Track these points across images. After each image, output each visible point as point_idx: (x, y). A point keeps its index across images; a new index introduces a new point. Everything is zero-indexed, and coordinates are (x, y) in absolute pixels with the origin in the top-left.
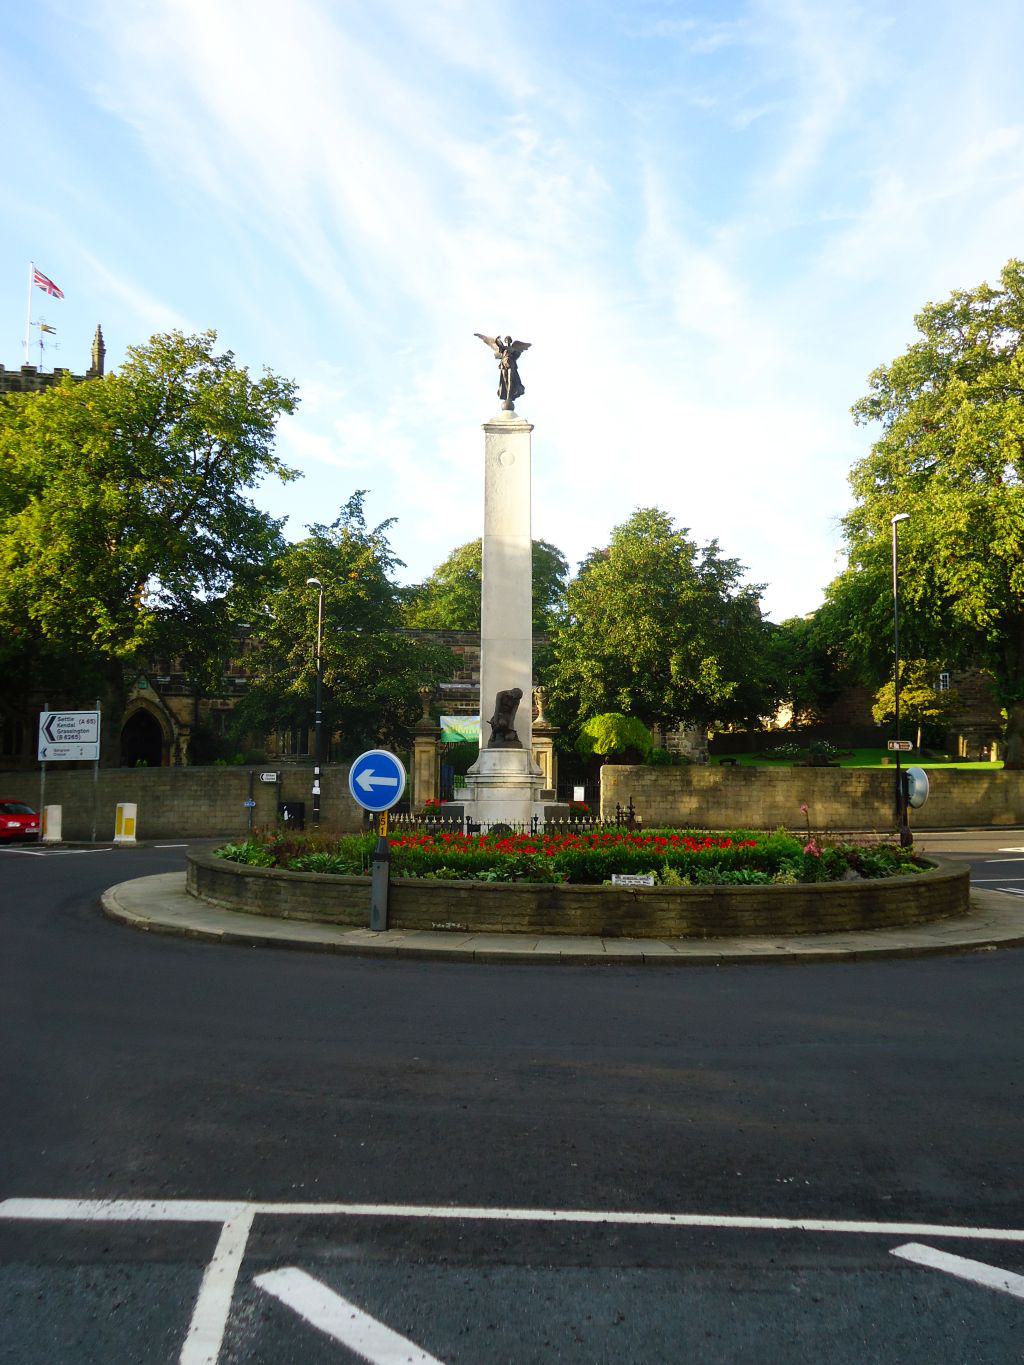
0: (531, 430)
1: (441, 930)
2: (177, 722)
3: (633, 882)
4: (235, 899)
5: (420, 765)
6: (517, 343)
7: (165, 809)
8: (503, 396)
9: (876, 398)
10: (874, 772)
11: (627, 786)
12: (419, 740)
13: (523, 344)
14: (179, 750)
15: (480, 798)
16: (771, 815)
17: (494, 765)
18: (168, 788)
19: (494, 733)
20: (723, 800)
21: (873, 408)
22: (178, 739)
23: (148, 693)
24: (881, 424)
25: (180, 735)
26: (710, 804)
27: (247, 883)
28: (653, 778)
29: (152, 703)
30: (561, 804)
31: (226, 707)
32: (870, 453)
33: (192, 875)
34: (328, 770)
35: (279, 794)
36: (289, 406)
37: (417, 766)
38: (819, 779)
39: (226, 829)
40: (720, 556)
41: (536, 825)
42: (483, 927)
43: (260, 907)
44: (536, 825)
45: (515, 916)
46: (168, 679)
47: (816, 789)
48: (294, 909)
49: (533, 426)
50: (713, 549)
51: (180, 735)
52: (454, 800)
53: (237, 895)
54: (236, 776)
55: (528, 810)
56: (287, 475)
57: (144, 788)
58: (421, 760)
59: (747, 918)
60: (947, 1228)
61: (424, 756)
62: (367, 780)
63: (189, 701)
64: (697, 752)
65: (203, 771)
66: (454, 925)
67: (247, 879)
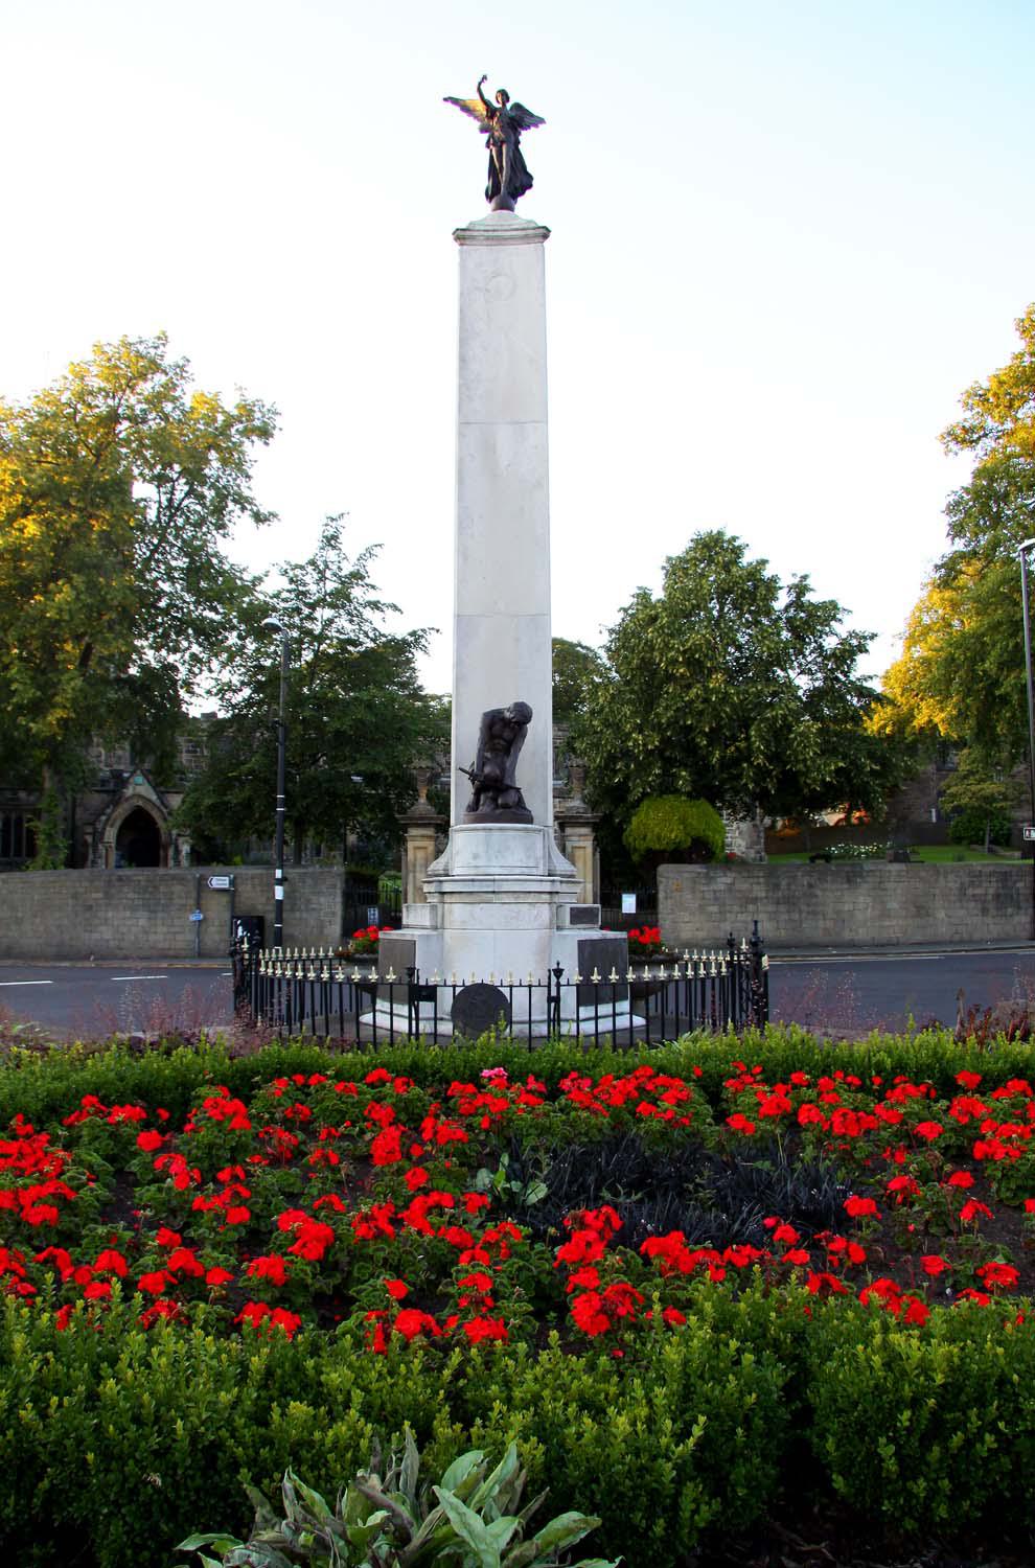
5: (414, 866)
9: (967, 425)
10: (1008, 869)
11: (694, 892)
12: (413, 832)
13: (532, 115)
14: (177, 851)
15: (447, 925)
16: (882, 927)
18: (100, 895)
19: (477, 794)
20: (820, 908)
21: (966, 437)
24: (973, 454)
25: (179, 835)
26: (804, 915)
28: (729, 881)
29: (150, 801)
30: (610, 934)
32: (970, 481)
34: (293, 873)
35: (233, 905)
36: (265, 433)
37: (411, 868)
38: (941, 879)
39: (169, 949)
40: (809, 597)
41: (558, 985)
44: (558, 985)
47: (937, 891)
50: (801, 589)
51: (179, 835)
54: (181, 880)
55: (546, 949)
56: (259, 518)
57: (75, 896)
58: (415, 860)
64: (752, 851)
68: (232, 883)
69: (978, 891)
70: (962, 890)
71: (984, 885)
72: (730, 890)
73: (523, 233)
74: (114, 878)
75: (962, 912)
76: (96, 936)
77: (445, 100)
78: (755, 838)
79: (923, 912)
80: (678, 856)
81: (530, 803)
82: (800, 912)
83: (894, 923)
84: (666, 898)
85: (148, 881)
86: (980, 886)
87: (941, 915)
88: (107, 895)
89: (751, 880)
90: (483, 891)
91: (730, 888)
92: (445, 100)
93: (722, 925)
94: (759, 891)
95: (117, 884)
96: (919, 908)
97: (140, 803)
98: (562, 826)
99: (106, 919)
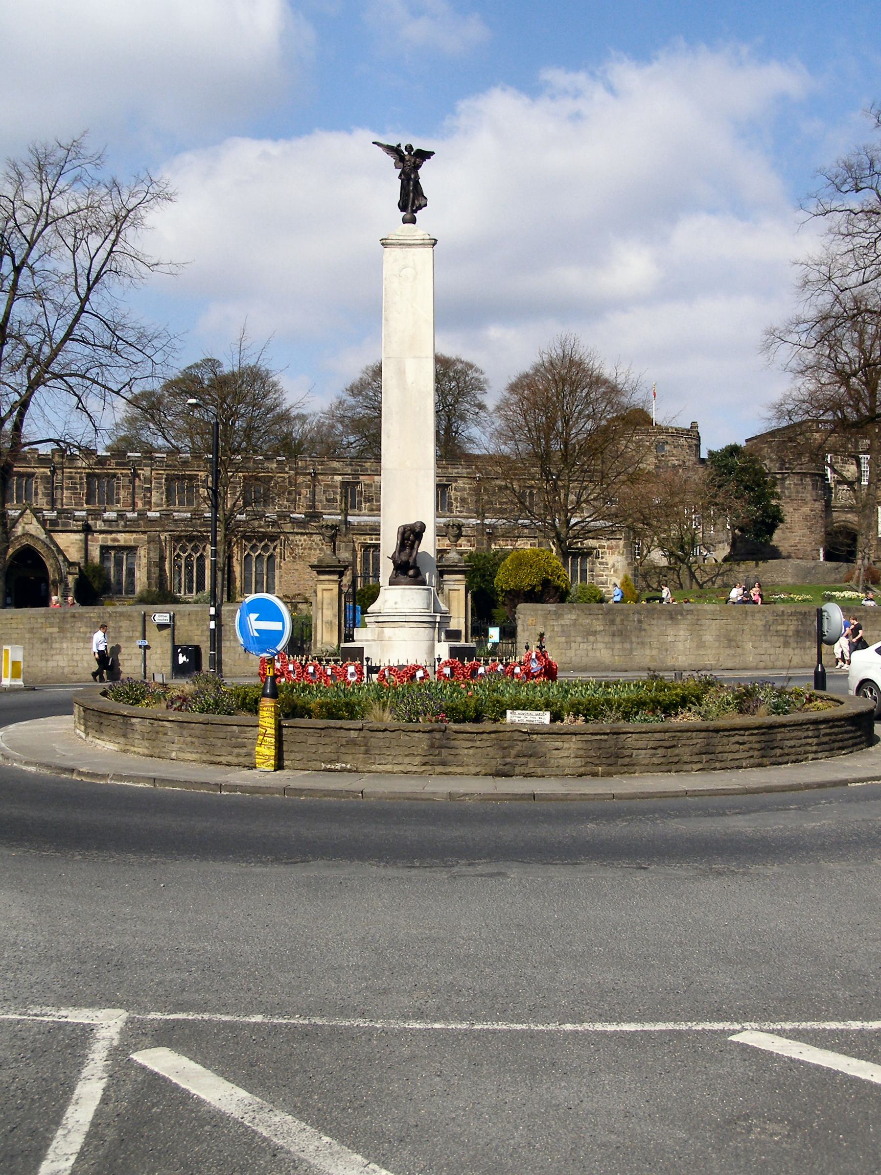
0: (434, 245)
1: (330, 770)
2: (66, 559)
3: (529, 718)
4: (122, 740)
7: (54, 652)
8: (403, 207)
17: (396, 603)
18: (56, 630)
23: (35, 528)
26: (634, 645)
27: (132, 724)
31: (116, 544)
33: (79, 718)
38: (749, 618)
43: (147, 748)
45: (407, 756)
46: (55, 513)
47: (745, 627)
48: (181, 750)
49: (436, 240)
52: (353, 641)
53: (125, 736)
54: (129, 617)
57: (31, 630)
59: (643, 756)
60: (854, 1061)
61: (327, 595)
62: (256, 624)
63: (79, 537)
65: (93, 612)
66: (344, 765)
67: (134, 720)
68: (172, 618)
69: (780, 628)
70: (767, 627)
72: (574, 625)
73: (450, 769)
74: (68, 615)
75: (766, 645)
76: (54, 664)
77: (373, 143)
79: (733, 644)
80: (533, 596)
82: (631, 643)
83: (709, 652)
84: (523, 630)
85: (99, 617)
86: (783, 624)
87: (749, 646)
88: (62, 630)
89: (592, 617)
90: (401, 621)
91: (575, 623)
92: (373, 143)
93: (567, 652)
94: (598, 626)
95: (70, 620)
96: (730, 640)
97: (31, 542)
98: (441, 574)
99: (61, 649)
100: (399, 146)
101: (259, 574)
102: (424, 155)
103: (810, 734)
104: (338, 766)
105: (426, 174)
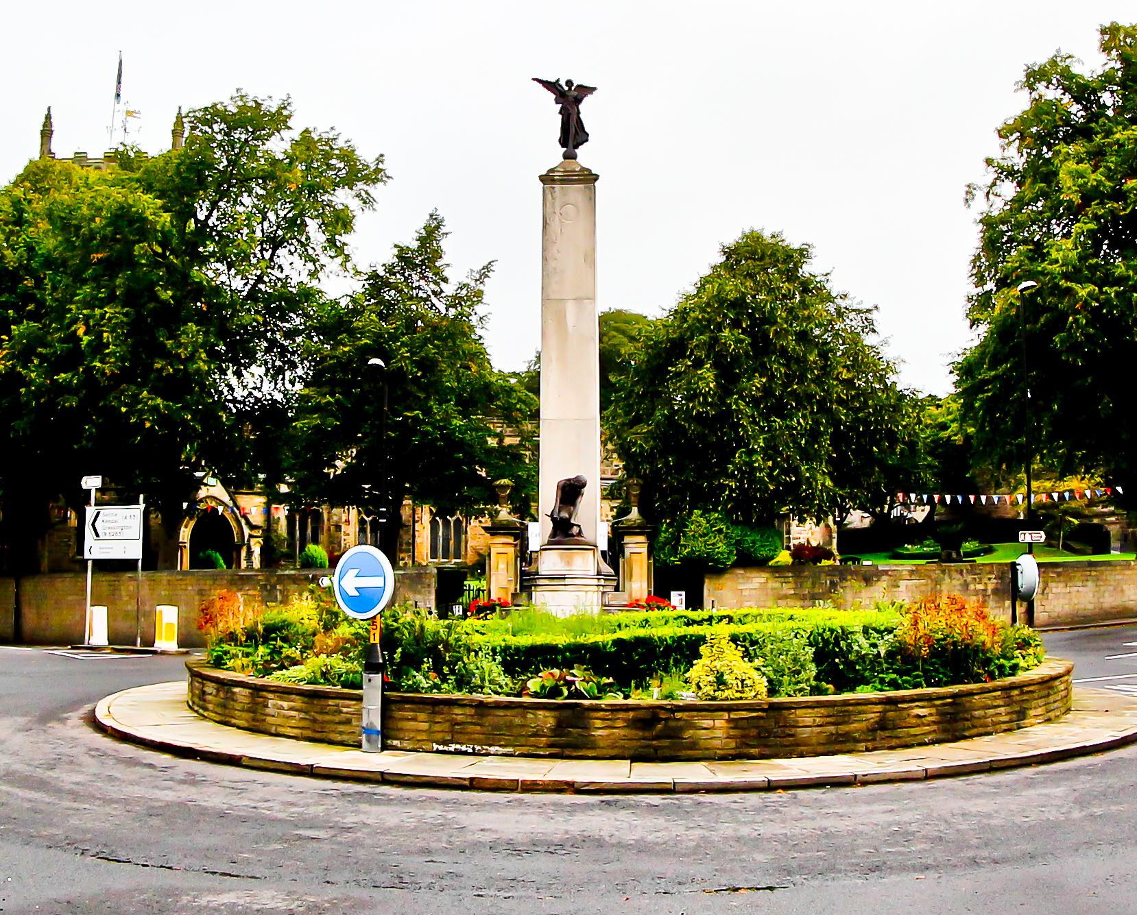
2: (248, 523)
6: (580, 87)
8: (564, 142)
14: (250, 553)
22: (249, 540)
25: (251, 536)
27: (234, 693)
28: (763, 580)
42: (492, 749)
67: (236, 690)
71: (985, 580)
77: (534, 79)
78: (827, 538)
81: (588, 535)
92: (534, 79)
100: (558, 80)
101: (446, 540)
102: (585, 90)
103: (1000, 702)
104: (452, 747)
105: (588, 110)
